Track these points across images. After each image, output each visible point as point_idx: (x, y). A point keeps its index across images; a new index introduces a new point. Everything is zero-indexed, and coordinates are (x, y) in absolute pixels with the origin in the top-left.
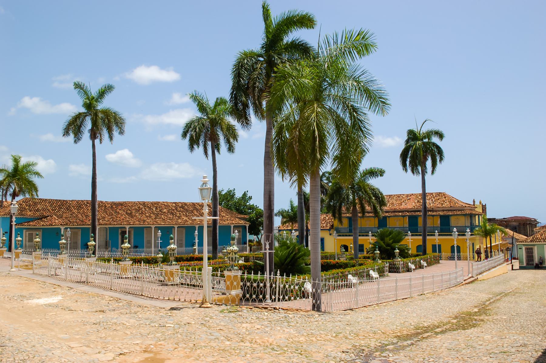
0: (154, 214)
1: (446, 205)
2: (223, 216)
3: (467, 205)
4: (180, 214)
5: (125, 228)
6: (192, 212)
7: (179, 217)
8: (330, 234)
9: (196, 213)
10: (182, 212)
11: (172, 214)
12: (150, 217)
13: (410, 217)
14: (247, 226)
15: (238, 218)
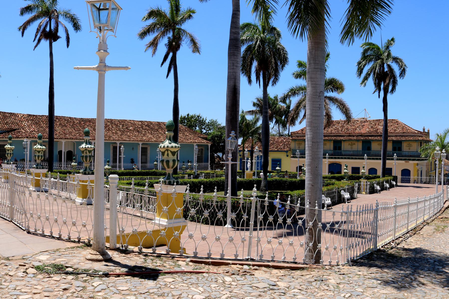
0: (120, 131)
1: (399, 130)
2: (187, 135)
3: (416, 132)
4: (145, 132)
5: (116, 143)
6: (157, 130)
7: (144, 135)
8: (287, 156)
9: (160, 132)
10: (147, 130)
11: (138, 132)
12: (116, 133)
13: (364, 142)
14: (209, 145)
15: (201, 137)
